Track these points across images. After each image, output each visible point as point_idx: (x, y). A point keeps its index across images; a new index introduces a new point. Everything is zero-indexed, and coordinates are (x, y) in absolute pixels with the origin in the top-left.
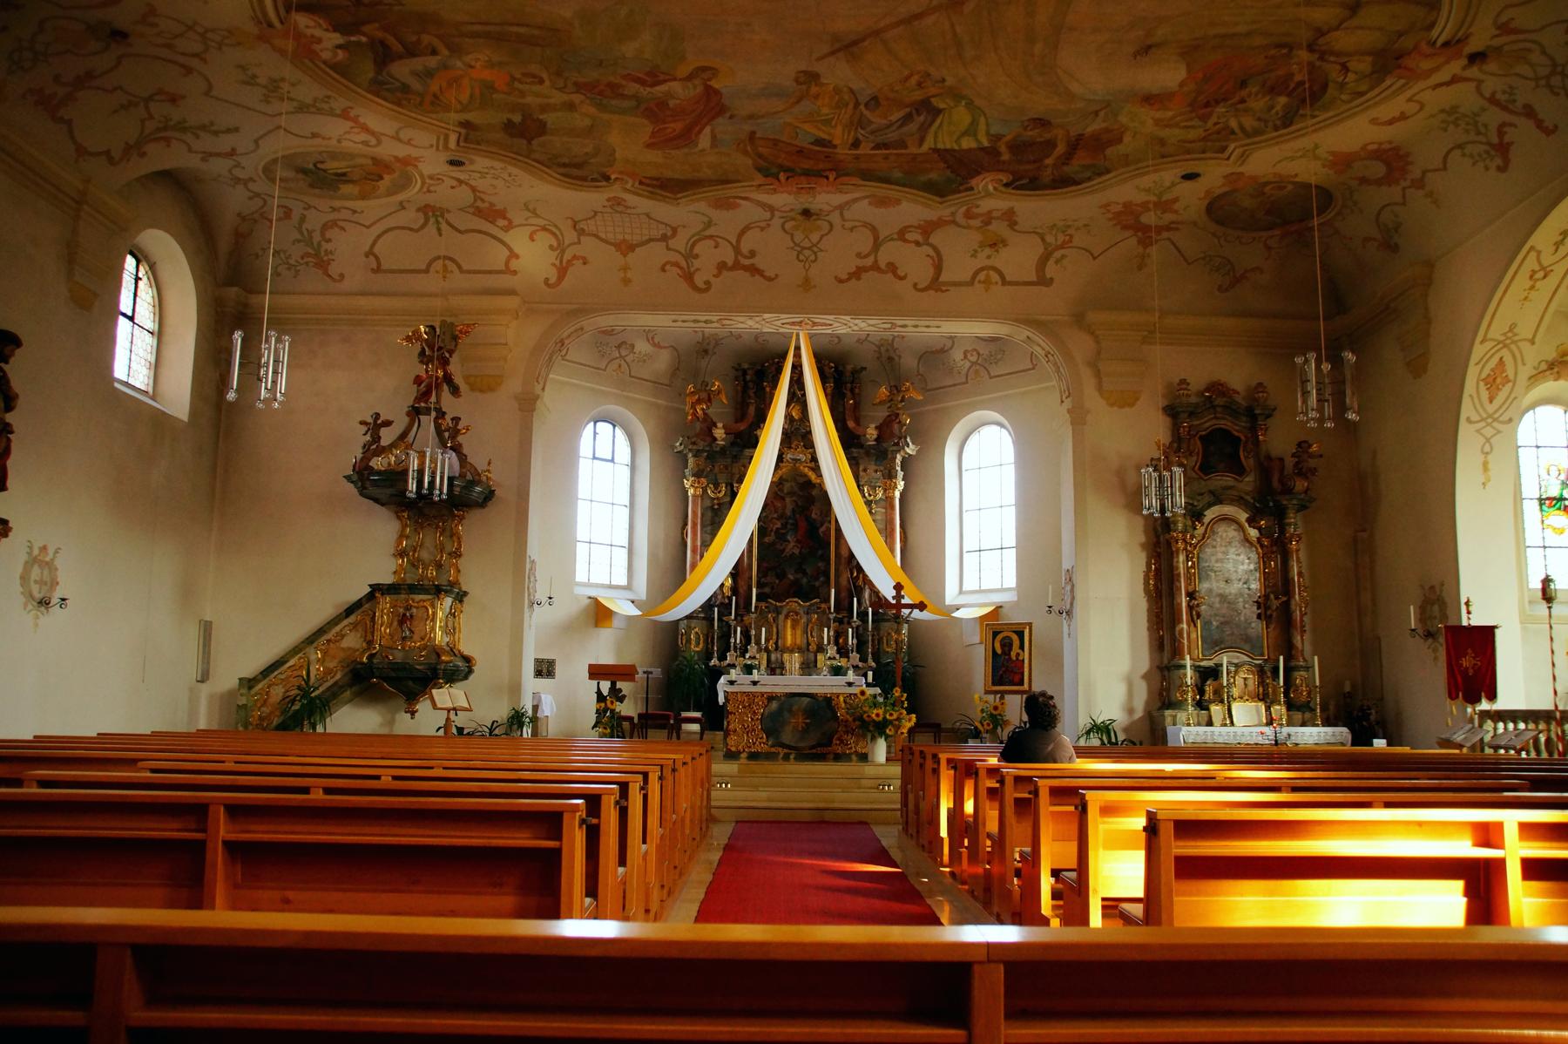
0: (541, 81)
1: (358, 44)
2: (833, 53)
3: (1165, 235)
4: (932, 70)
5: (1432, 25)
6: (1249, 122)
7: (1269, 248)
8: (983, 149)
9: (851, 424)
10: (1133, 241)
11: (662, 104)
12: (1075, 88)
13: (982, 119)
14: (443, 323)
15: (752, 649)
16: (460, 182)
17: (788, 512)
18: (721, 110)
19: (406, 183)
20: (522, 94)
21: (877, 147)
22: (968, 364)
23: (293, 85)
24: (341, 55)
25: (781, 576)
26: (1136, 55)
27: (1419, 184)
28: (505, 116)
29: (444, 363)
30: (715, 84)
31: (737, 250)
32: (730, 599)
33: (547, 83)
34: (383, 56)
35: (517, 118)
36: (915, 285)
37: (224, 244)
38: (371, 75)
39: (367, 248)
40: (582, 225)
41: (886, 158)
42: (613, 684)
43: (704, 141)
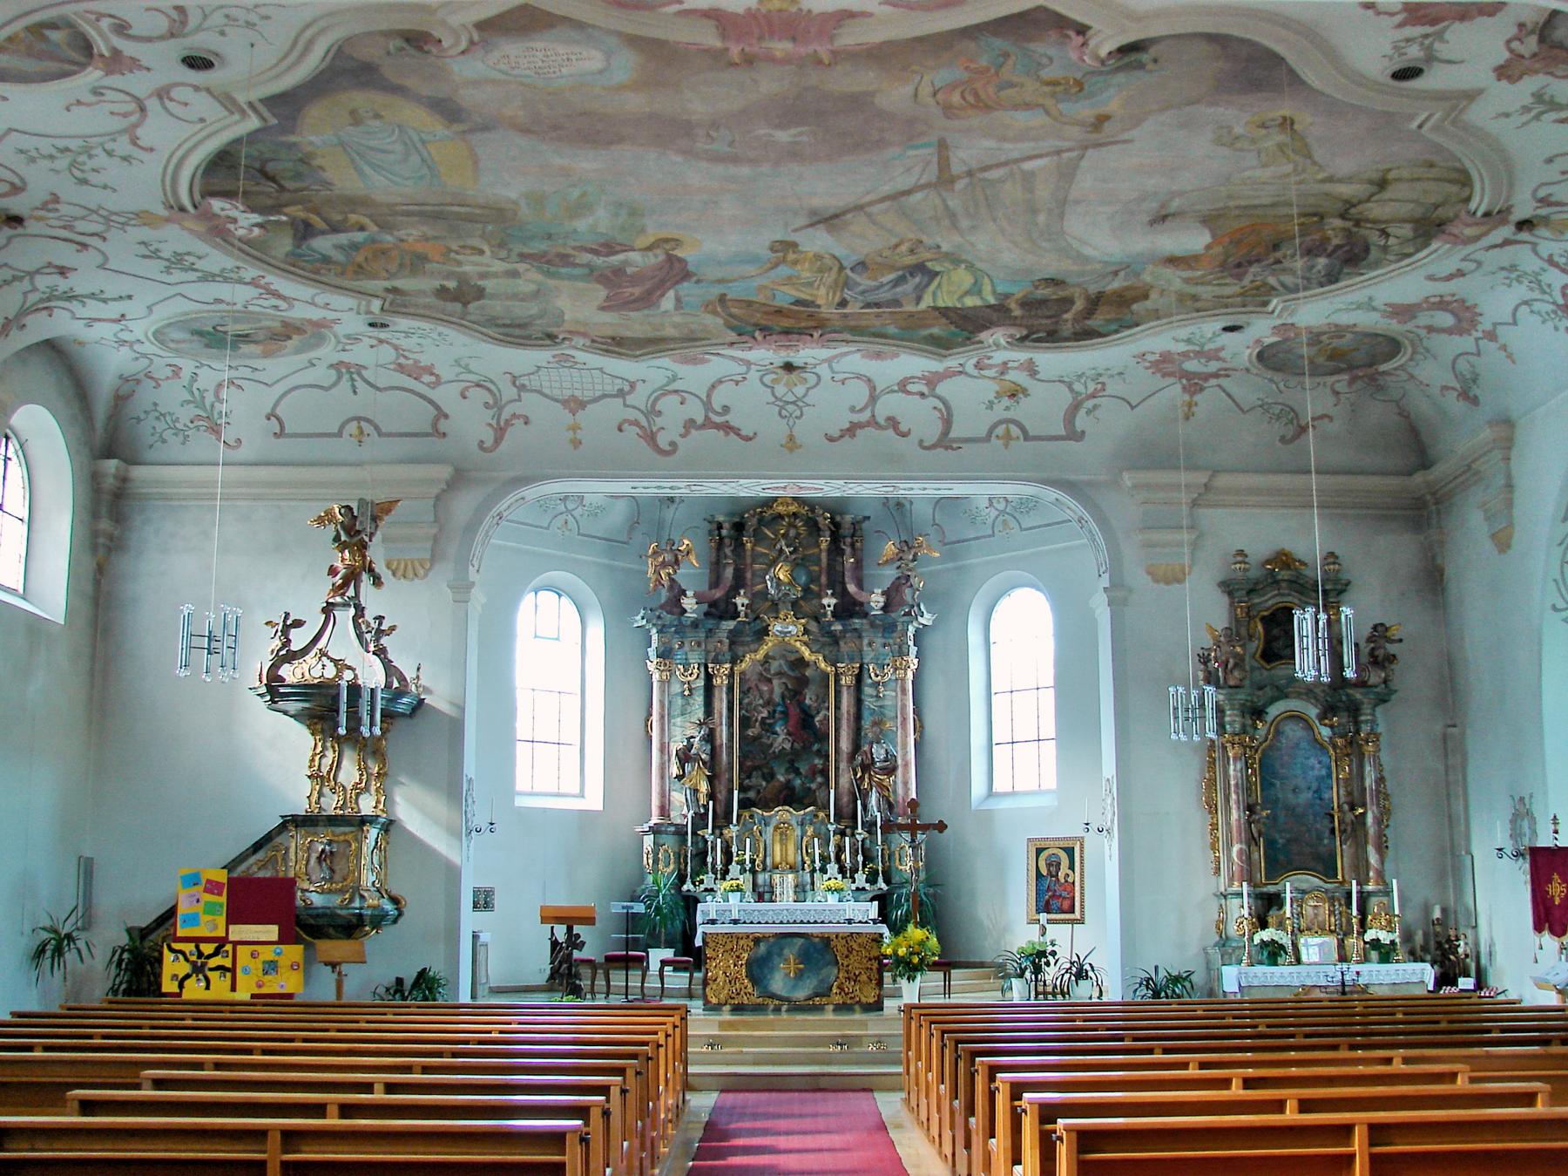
0: (481, 252)
1: (278, 223)
2: (812, 225)
3: (1213, 382)
4: (924, 238)
5: (1468, 199)
6: (1288, 279)
7: (1337, 393)
8: (990, 307)
9: (852, 588)
10: (1178, 387)
11: (619, 271)
12: (1088, 251)
13: (986, 280)
14: (362, 502)
15: (734, 868)
16: (381, 341)
17: (777, 698)
18: (687, 276)
19: (319, 340)
20: (459, 263)
21: (868, 305)
22: (994, 513)
23: (199, 258)
24: (257, 231)
25: (770, 777)
26: (1152, 223)
27: (1491, 336)
28: (437, 284)
29: (363, 546)
30: (679, 253)
31: (707, 405)
32: (706, 807)
33: (488, 253)
34: (304, 231)
35: (452, 284)
36: (921, 441)
37: (101, 409)
38: (289, 248)
39: (268, 410)
40: (524, 381)
41: (878, 316)
42: (570, 929)
43: (668, 302)
